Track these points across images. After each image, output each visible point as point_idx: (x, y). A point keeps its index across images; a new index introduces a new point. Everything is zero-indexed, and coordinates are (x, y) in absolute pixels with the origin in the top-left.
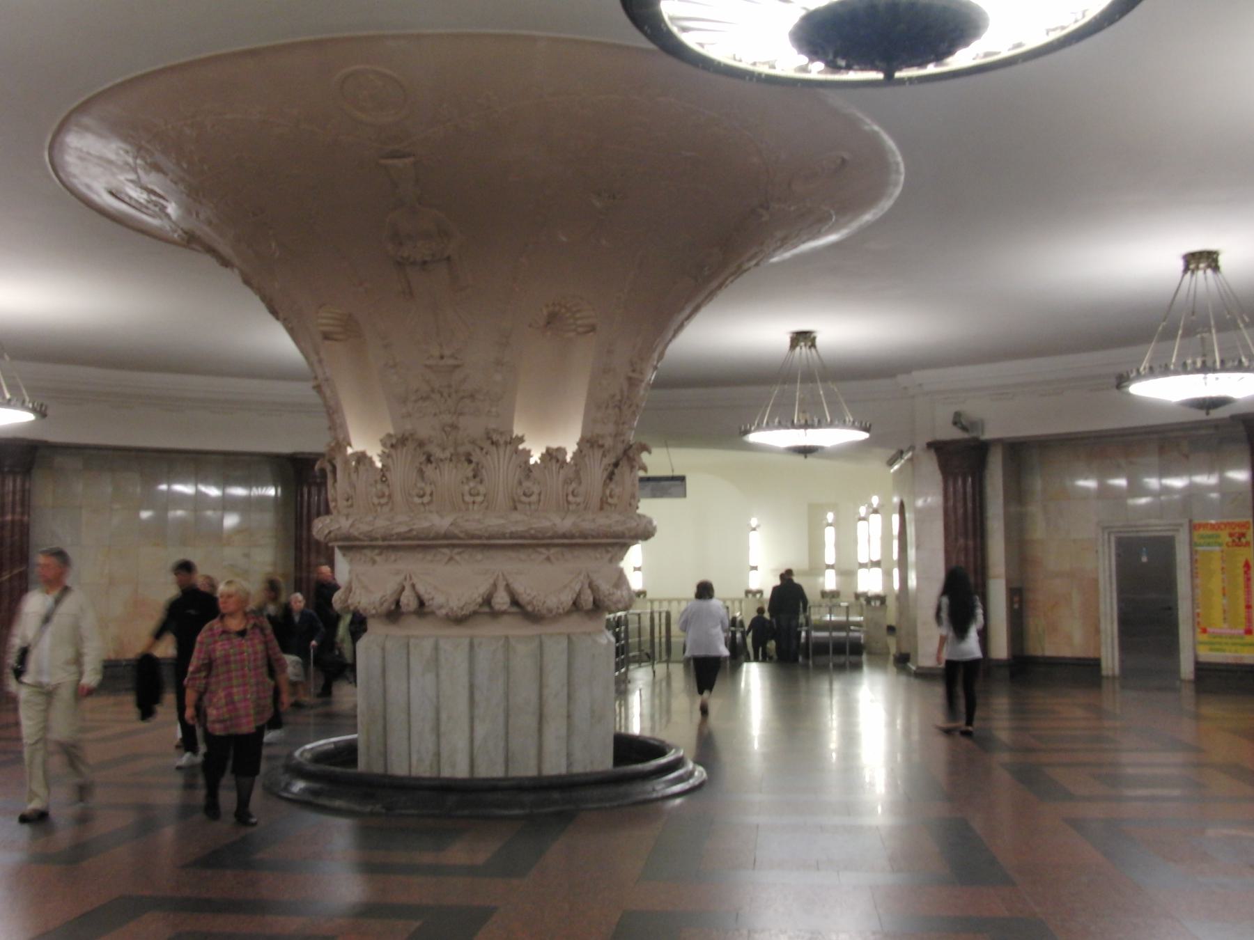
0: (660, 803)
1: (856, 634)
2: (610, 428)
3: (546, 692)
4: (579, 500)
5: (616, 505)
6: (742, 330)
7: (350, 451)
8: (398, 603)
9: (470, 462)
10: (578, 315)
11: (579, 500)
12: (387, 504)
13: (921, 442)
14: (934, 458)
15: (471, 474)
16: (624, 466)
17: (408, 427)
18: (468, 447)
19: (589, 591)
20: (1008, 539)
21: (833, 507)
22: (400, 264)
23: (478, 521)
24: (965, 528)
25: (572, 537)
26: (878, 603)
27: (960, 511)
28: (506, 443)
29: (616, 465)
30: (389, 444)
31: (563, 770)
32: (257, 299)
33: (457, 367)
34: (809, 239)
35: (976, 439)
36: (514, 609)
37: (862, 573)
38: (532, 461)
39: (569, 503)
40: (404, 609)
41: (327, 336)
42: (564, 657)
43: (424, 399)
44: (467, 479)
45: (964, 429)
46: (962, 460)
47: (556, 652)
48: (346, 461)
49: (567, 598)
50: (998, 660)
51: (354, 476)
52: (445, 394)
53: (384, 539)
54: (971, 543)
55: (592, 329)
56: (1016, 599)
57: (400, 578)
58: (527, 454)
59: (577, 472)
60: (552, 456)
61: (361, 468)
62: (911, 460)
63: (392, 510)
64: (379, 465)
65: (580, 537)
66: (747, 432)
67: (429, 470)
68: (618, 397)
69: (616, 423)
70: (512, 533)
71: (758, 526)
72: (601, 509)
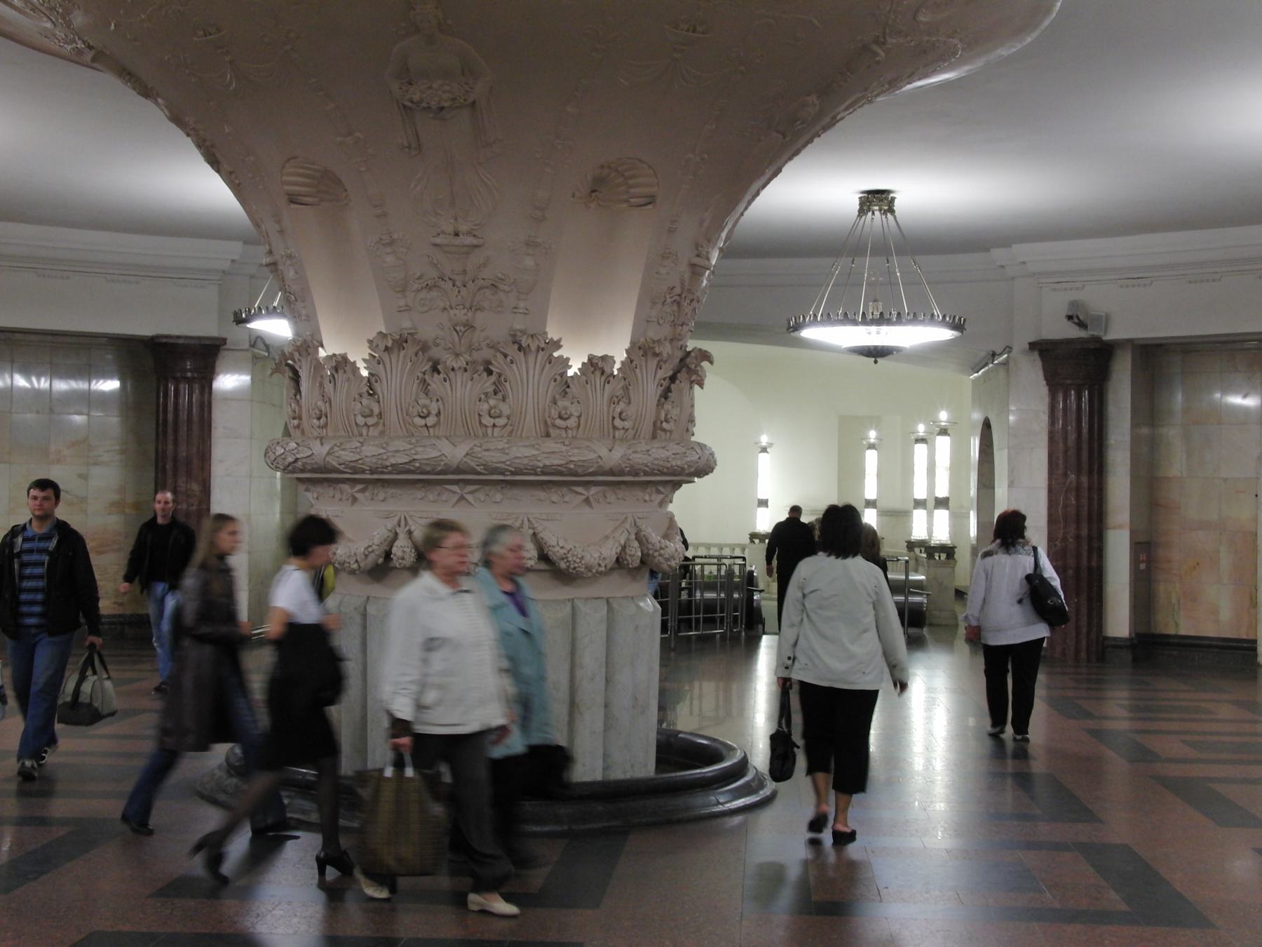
0: (719, 821)
1: (917, 599)
2: (666, 331)
3: (579, 673)
4: (627, 424)
5: (671, 432)
6: (814, 190)
7: (322, 353)
8: (388, 555)
9: (490, 373)
10: (631, 182)
11: (627, 424)
12: (376, 425)
13: (1021, 342)
14: (1039, 363)
15: (491, 390)
16: (682, 383)
17: (406, 324)
18: (486, 353)
19: (636, 544)
20: (1134, 478)
21: (875, 422)
22: (407, 110)
23: (502, 451)
24: (1078, 462)
25: (622, 473)
26: (943, 556)
27: (1072, 437)
28: (539, 349)
29: (673, 379)
30: (382, 347)
31: (598, 776)
32: (189, 142)
33: (477, 246)
34: (920, 79)
35: (1097, 340)
36: (543, 566)
37: (919, 516)
38: (570, 373)
39: (615, 428)
40: (396, 563)
41: (293, 199)
42: (603, 627)
43: (429, 288)
44: (486, 394)
45: (1082, 325)
46: (1078, 366)
47: (592, 619)
48: (318, 366)
49: (610, 551)
50: (1115, 639)
51: (329, 388)
52: (458, 283)
53: (372, 472)
54: (1085, 480)
55: (651, 200)
56: (1143, 557)
57: (391, 524)
58: (565, 363)
59: (626, 389)
60: (596, 366)
61: (340, 377)
62: (1005, 364)
63: (382, 433)
64: (365, 373)
65: (629, 474)
66: (798, 327)
67: (435, 382)
68: (678, 290)
69: (674, 324)
70: (545, 466)
71: (771, 445)
72: (654, 437)
